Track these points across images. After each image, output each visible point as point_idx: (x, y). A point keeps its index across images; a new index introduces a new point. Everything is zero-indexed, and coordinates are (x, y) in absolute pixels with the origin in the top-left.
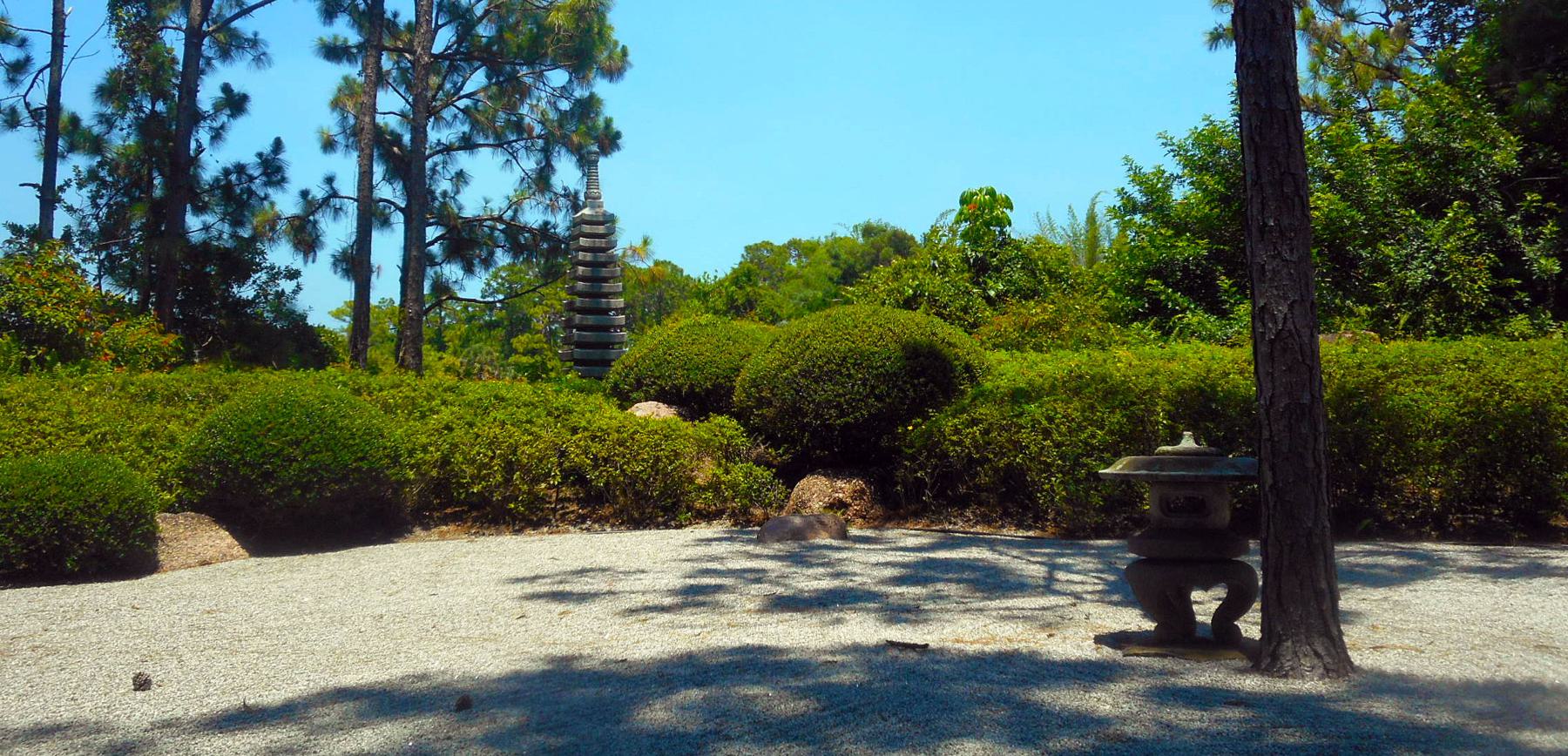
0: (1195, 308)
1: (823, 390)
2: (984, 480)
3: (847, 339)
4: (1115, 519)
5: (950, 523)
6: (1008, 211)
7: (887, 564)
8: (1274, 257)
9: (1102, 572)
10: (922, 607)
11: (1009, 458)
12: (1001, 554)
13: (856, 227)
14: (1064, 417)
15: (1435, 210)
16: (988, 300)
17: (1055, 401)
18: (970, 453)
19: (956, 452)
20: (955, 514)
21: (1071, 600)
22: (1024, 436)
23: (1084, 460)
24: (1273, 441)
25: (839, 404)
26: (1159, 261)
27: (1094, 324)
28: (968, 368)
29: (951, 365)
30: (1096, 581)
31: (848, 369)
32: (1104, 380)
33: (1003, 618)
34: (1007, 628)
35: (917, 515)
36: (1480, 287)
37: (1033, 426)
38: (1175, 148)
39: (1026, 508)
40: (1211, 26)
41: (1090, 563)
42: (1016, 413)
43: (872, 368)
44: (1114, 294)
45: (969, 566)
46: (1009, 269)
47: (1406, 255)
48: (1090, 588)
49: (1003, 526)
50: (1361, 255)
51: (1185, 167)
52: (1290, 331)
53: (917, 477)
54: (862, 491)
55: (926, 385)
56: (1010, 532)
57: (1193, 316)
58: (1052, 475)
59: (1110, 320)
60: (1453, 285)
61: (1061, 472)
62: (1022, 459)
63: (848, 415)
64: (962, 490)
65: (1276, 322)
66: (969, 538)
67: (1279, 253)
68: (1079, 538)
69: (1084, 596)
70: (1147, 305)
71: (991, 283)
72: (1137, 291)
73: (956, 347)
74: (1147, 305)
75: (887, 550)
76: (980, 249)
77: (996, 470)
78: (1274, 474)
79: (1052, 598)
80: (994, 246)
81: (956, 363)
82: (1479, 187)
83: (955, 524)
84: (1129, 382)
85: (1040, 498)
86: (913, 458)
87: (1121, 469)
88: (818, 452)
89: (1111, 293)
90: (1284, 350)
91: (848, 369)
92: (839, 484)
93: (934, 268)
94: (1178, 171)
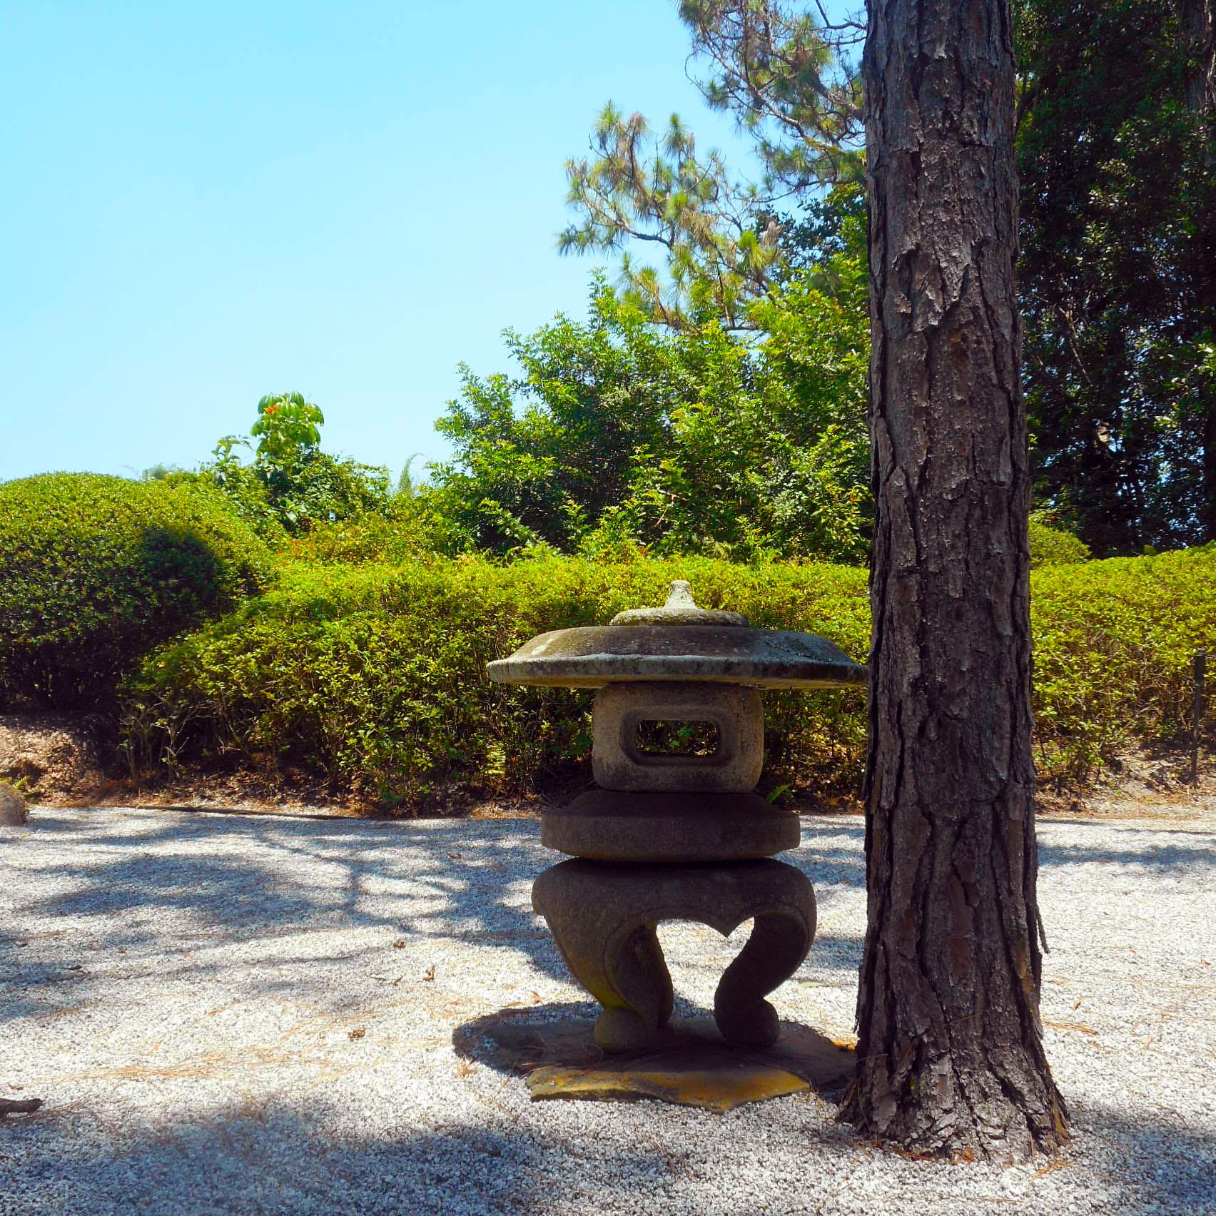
0: (537, 538)
1: (11, 590)
2: (258, 734)
3: (58, 516)
4: (447, 789)
5: (203, 797)
6: (317, 425)
7: (57, 871)
8: (942, 136)
9: (441, 873)
10: (90, 968)
11: (298, 699)
12: (273, 845)
13: (146, 472)
14: (381, 639)
15: (807, 437)
16: (288, 525)
17: (370, 618)
18: (239, 691)
19: (218, 689)
20: (213, 783)
21: (394, 935)
22: (323, 667)
23: (408, 702)
24: (925, 575)
25: (36, 613)
26: (496, 482)
27: (415, 553)
28: (245, 571)
29: (220, 565)
30: (434, 892)
31: (53, 560)
32: (439, 591)
33: (258, 989)
34: (261, 1015)
35: (152, 786)
36: (849, 524)
37: (336, 652)
38: (521, 349)
39: (320, 774)
40: (562, 227)
41: (419, 859)
42: (312, 632)
43: (93, 559)
44: (441, 518)
45: (213, 869)
46: (314, 489)
47: (772, 487)
48: (426, 907)
49: (283, 801)
50: (730, 479)
51: (532, 372)
52: (974, 309)
53: (155, 728)
54: (68, 750)
55: (177, 589)
56: (295, 810)
57: (534, 546)
58: (360, 725)
59: (434, 548)
60: (823, 521)
61: (374, 720)
62: (317, 700)
63: (50, 630)
64: (225, 748)
65: (944, 289)
66: (229, 820)
67: (955, 128)
68: (394, 817)
69: (417, 923)
70: (479, 535)
71: (291, 504)
72: (467, 518)
73: (231, 540)
74: (479, 535)
75: (78, 842)
76: (281, 461)
77: (279, 719)
78: (924, 652)
79: (359, 931)
80: (298, 460)
81: (228, 561)
82: (848, 416)
83: (210, 798)
84: (474, 595)
85: (340, 759)
86: (151, 699)
87: (544, 654)
88: (18, 696)
89: (438, 517)
90: (960, 354)
91: (53, 560)
92: (31, 738)
93: (221, 482)
94: (522, 376)
